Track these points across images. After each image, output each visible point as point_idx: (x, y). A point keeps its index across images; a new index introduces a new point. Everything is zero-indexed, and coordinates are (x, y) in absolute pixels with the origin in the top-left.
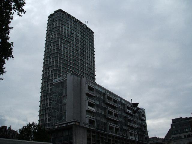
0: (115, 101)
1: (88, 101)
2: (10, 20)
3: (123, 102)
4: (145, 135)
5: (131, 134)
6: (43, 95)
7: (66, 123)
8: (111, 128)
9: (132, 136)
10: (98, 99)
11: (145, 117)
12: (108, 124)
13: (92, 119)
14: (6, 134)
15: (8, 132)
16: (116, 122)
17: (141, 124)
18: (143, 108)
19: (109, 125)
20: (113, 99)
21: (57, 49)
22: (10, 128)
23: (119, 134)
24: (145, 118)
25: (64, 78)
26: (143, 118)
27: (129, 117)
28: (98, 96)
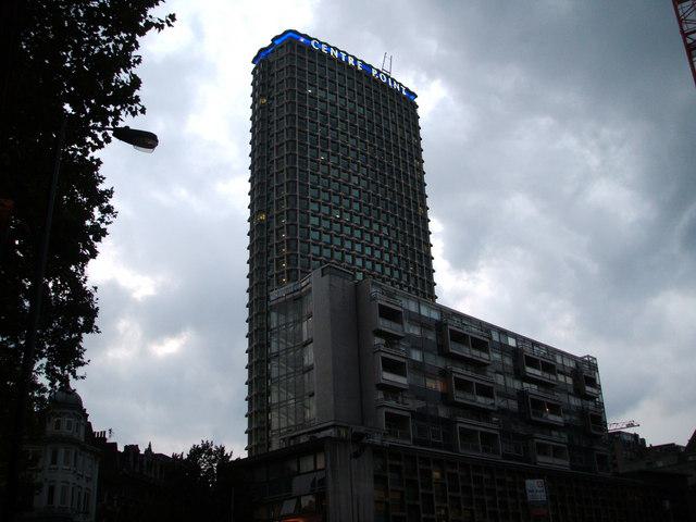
0: (480, 345)
1: (383, 354)
2: (121, 449)
3: (512, 342)
4: (596, 447)
5: (542, 449)
6: (256, 363)
7: (309, 433)
8: (467, 435)
9: (545, 454)
10: (417, 344)
11: (598, 387)
12: (456, 422)
13: (397, 412)
14: (137, 470)
15: (145, 463)
16: (481, 413)
17: (582, 412)
18: (588, 356)
19: (458, 425)
20: (472, 338)
21: (290, 171)
22: (149, 450)
23: (496, 452)
24: (595, 391)
25: (303, 284)
26: (588, 389)
27: (460, 370)
28: (416, 331)
